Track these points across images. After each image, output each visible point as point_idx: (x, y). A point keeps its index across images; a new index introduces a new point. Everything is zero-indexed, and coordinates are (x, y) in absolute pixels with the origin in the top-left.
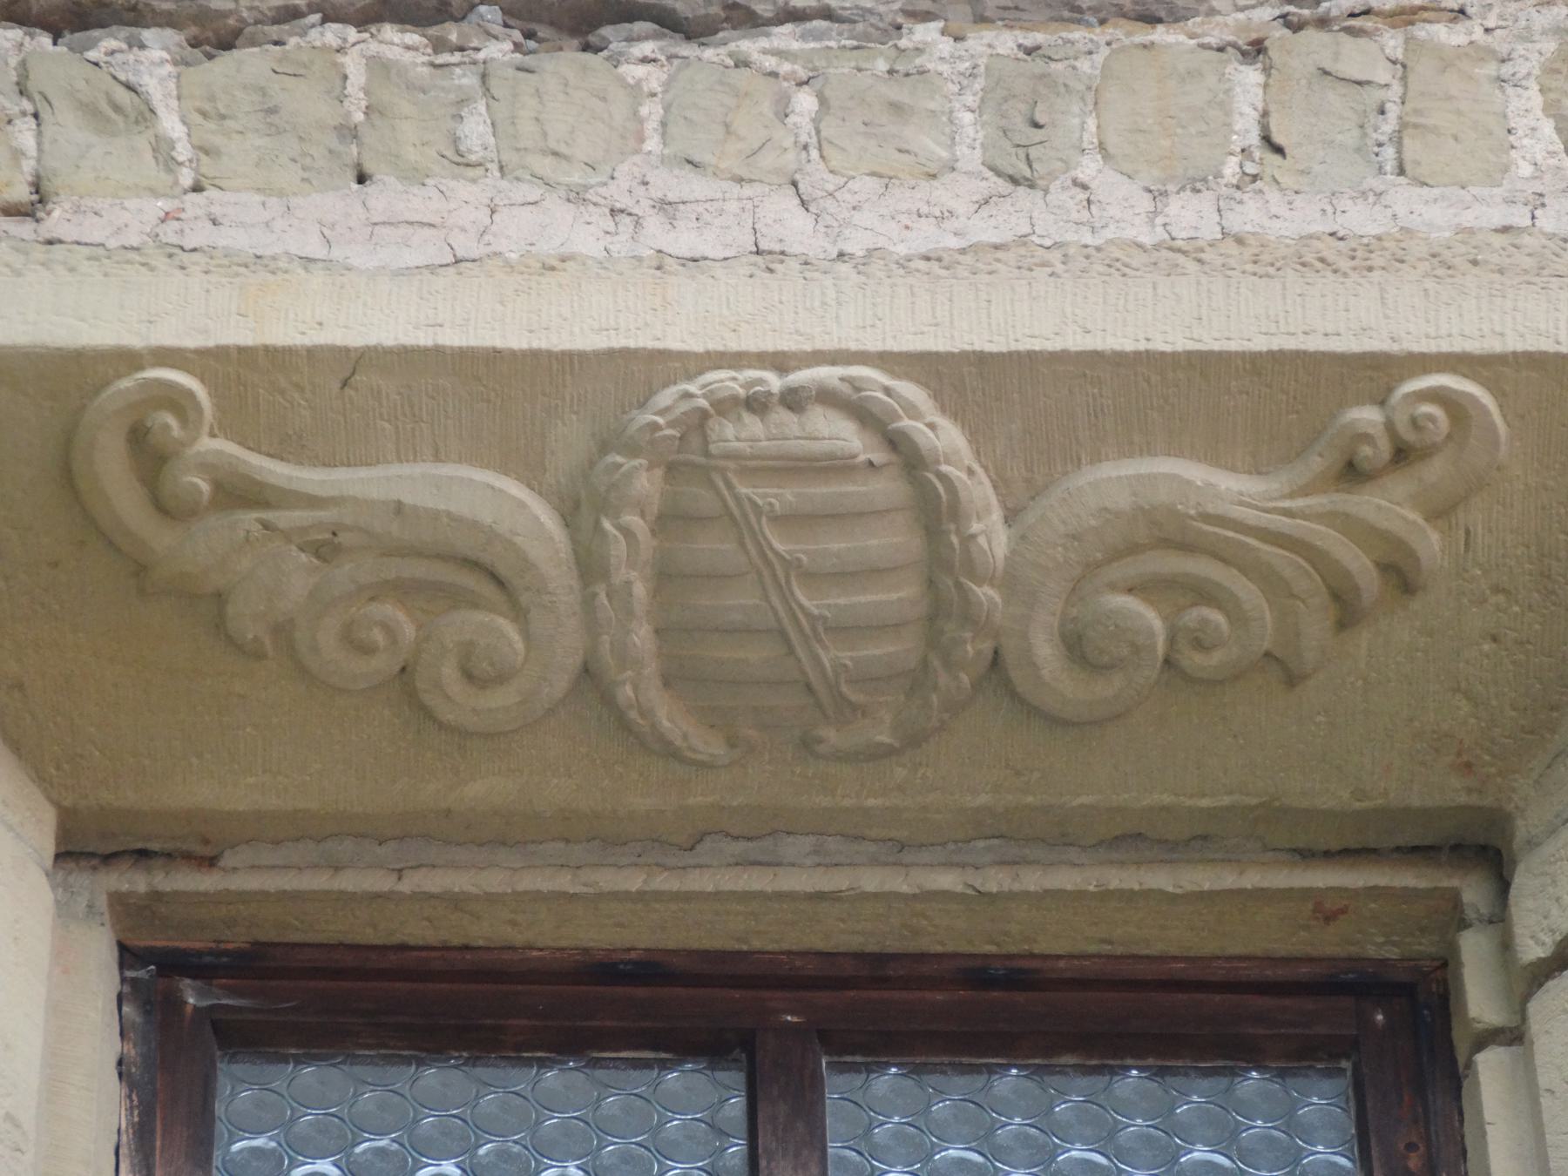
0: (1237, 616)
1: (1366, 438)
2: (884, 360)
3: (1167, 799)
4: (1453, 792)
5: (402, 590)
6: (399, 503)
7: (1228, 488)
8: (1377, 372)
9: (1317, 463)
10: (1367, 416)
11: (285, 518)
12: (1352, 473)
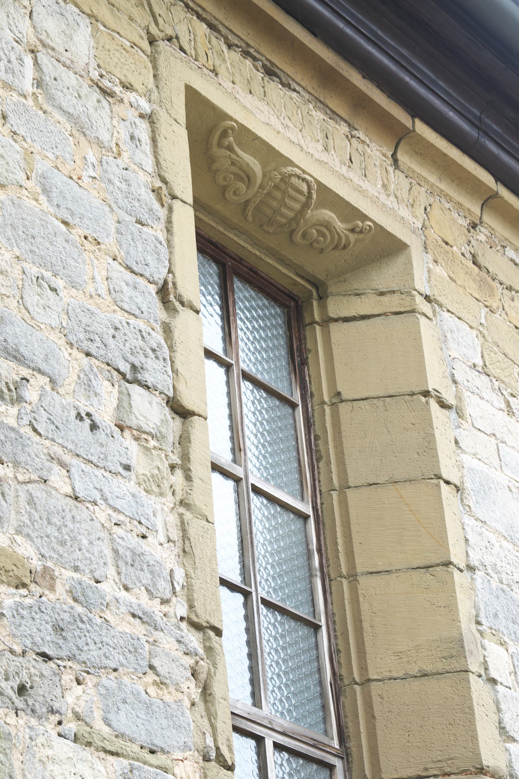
0: (325, 241)
1: (358, 227)
2: (315, 179)
3: (292, 259)
4: (322, 277)
5: (236, 175)
6: (248, 164)
7: (340, 225)
8: (365, 217)
9: (350, 226)
10: (360, 223)
11: (233, 156)
12: (352, 231)
